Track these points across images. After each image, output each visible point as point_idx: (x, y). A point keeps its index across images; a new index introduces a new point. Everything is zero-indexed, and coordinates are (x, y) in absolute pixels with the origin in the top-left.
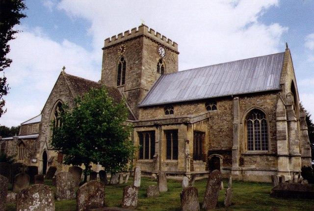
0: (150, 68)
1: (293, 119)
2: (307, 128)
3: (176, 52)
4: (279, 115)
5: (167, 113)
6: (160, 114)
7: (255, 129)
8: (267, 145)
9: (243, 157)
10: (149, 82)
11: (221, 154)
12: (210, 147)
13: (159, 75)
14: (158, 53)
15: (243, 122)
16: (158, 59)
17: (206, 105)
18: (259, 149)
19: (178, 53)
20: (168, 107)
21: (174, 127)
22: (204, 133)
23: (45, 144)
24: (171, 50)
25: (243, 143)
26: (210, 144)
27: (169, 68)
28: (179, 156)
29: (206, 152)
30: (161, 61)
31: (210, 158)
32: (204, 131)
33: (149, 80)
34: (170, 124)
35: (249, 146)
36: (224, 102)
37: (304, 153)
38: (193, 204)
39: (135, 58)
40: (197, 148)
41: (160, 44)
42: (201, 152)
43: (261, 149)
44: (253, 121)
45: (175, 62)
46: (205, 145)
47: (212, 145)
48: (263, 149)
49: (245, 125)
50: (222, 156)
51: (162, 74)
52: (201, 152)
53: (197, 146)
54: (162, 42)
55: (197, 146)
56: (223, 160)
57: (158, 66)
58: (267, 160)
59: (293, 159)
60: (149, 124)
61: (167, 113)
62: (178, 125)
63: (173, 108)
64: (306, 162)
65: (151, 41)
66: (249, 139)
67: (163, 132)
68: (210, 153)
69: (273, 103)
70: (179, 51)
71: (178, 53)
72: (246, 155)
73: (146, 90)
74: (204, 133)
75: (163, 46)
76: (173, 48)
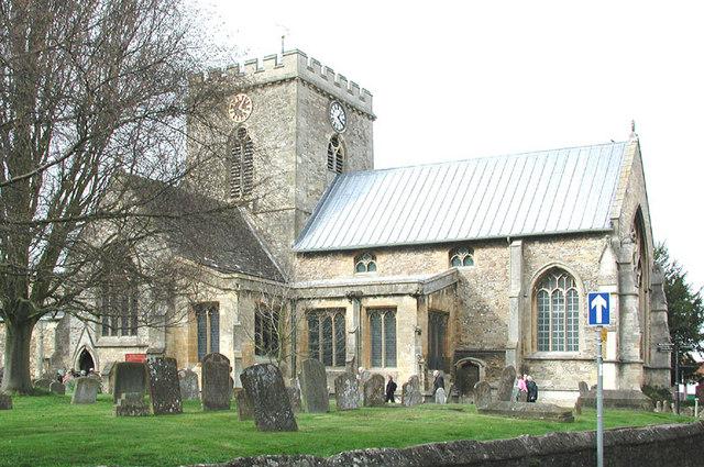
0: (314, 161)
1: (630, 292)
2: (665, 307)
3: (368, 115)
4: (604, 282)
5: (359, 268)
6: (344, 273)
7: (555, 308)
8: (576, 341)
9: (528, 364)
10: (312, 193)
11: (482, 357)
12: (460, 343)
13: (332, 176)
14: (329, 120)
15: (530, 294)
16: (329, 137)
17: (450, 255)
18: (561, 349)
19: (373, 118)
20: (363, 255)
21: (390, 302)
22: (448, 314)
23: (86, 333)
24: (358, 110)
25: (529, 336)
26: (458, 336)
27: (353, 153)
28: (398, 361)
29: (451, 354)
30: (335, 140)
31: (459, 364)
32: (446, 310)
33: (312, 188)
34: (379, 295)
35: (540, 341)
36: (490, 250)
37: (656, 360)
38: (403, 461)
39: (276, 133)
40: (433, 346)
41: (335, 98)
42: (440, 353)
43: (307, 410)
44: (550, 293)
45: (366, 140)
46: (449, 339)
47: (464, 340)
48: (569, 349)
49: (533, 300)
50: (485, 364)
51: (339, 172)
52: (440, 353)
53: (434, 341)
54: (338, 92)
55: (434, 341)
56: (487, 370)
57: (331, 153)
58: (577, 370)
59: (628, 367)
60: (333, 293)
61: (359, 268)
62: (396, 298)
63: (374, 258)
64: (660, 377)
65: (313, 92)
66: (540, 328)
67: (364, 311)
68: (459, 354)
69: (592, 257)
70: (375, 112)
71: (373, 118)
72: (532, 360)
73: (305, 213)
74: (448, 314)
75: (339, 102)
76: (362, 105)
